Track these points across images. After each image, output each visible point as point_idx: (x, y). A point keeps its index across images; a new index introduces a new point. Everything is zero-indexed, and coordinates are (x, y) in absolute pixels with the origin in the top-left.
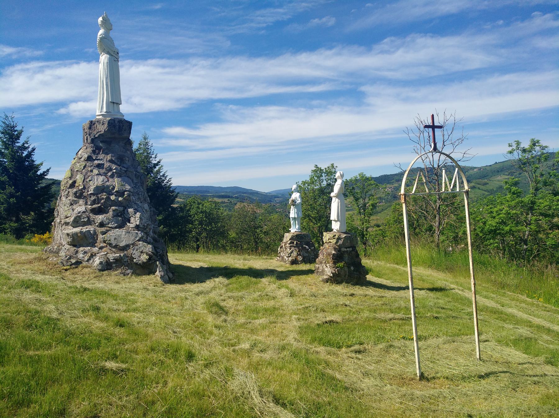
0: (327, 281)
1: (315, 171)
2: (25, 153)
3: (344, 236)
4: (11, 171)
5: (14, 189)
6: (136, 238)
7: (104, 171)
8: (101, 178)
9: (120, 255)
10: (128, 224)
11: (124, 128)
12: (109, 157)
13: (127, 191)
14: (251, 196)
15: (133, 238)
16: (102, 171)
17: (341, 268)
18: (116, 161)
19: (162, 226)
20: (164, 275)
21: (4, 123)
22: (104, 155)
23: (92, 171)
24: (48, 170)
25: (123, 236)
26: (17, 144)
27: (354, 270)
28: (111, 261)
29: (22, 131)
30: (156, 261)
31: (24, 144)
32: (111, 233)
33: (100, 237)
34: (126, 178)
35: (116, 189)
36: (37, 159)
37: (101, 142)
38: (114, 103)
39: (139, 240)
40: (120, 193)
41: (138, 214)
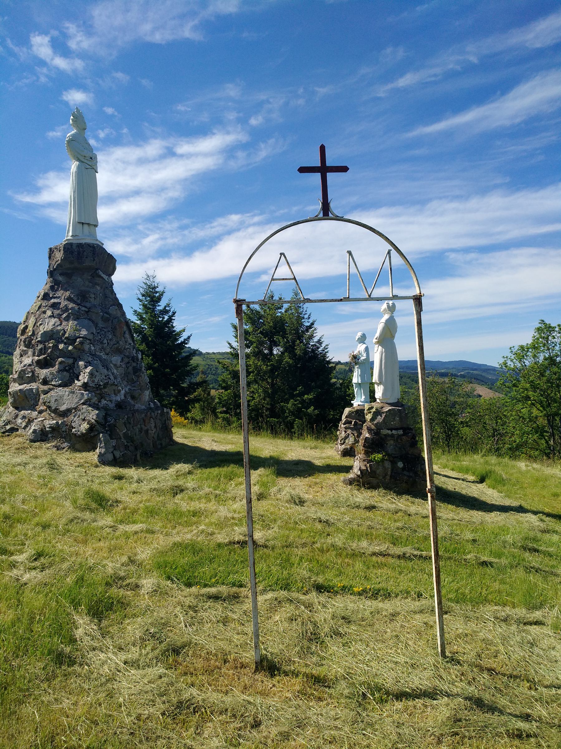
0: (351, 482)
1: (539, 330)
2: (166, 318)
3: (387, 408)
4: (150, 339)
5: (152, 360)
6: (80, 400)
7: (58, 312)
8: (53, 321)
9: (57, 423)
10: (76, 382)
11: (85, 254)
12: (68, 294)
13: (80, 337)
14: (483, 374)
15: (76, 400)
16: (57, 312)
17: (378, 462)
18: (75, 299)
19: (312, 408)
20: (105, 453)
21: (146, 284)
22: (62, 292)
23: (44, 312)
24: (189, 338)
25: (65, 398)
26: (158, 308)
27: (404, 469)
28: (47, 429)
29: (163, 292)
30: (99, 434)
31: (165, 307)
32: (52, 393)
33: (42, 396)
34: (86, 321)
35: (67, 335)
36: (178, 325)
37: (61, 274)
38: (83, 223)
39: (83, 404)
40: (71, 341)
41: (89, 369)
